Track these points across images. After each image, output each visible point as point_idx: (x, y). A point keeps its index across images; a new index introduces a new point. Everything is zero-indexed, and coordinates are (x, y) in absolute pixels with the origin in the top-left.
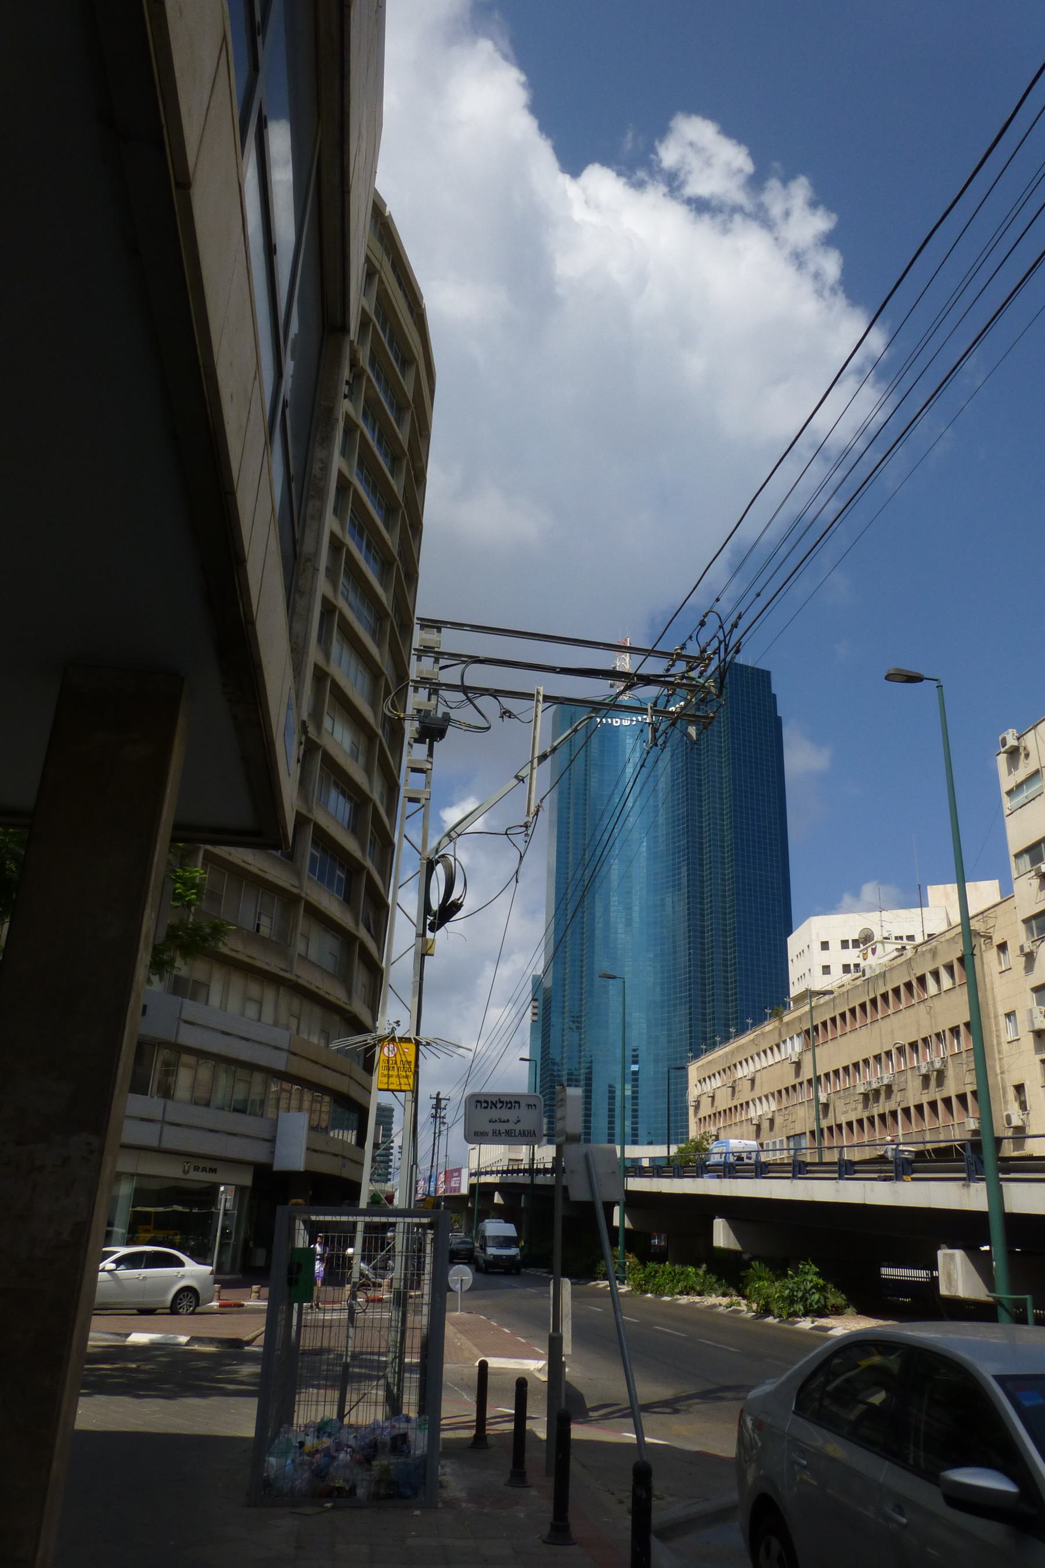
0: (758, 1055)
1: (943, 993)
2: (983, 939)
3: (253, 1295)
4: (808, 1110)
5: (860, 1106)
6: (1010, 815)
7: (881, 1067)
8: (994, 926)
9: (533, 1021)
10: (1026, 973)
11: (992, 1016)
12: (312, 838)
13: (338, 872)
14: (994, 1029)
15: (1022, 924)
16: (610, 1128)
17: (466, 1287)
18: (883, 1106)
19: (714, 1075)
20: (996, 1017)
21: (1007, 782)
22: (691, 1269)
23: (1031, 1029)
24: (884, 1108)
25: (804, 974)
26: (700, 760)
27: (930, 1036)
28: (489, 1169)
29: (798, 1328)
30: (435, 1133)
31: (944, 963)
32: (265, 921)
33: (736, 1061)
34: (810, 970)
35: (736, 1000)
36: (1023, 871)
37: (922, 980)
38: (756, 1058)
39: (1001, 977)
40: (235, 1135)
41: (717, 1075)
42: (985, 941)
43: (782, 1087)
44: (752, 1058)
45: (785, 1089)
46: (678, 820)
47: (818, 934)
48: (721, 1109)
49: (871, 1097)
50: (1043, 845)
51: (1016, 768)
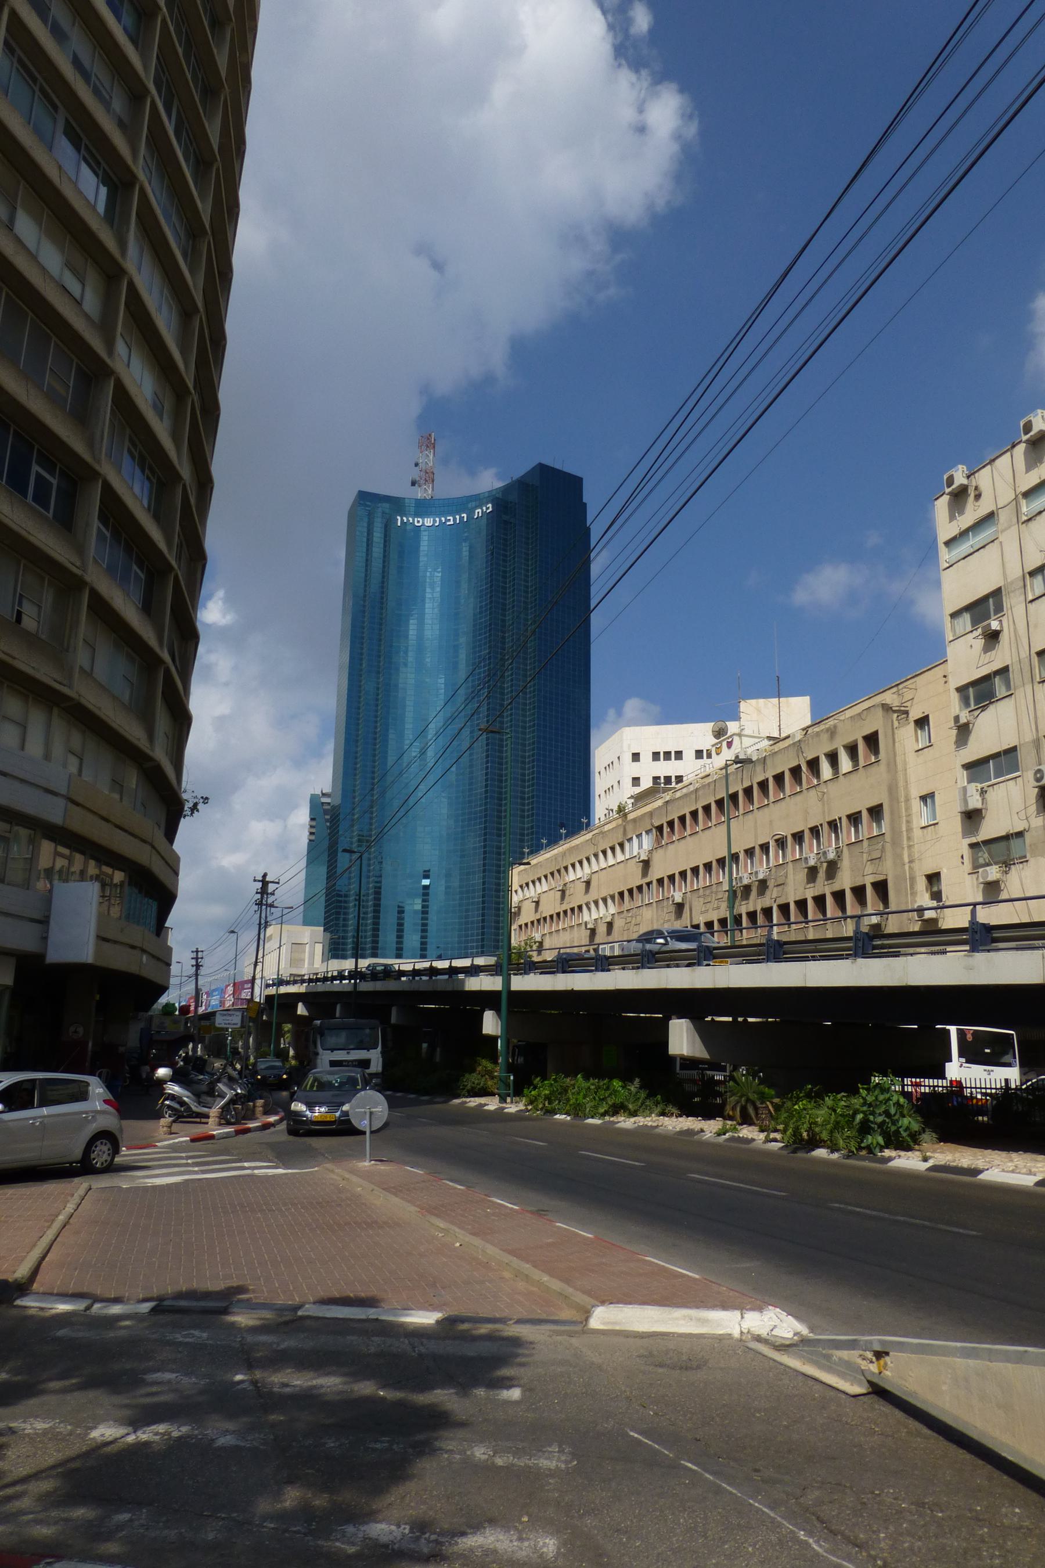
0: (596, 856)
1: (841, 776)
2: (895, 715)
4: (657, 910)
5: (724, 905)
7: (752, 863)
8: (913, 699)
9: (310, 840)
10: (957, 748)
11: (902, 799)
13: (135, 567)
14: (904, 813)
15: (956, 693)
16: (398, 943)
18: (755, 903)
19: (539, 879)
20: (907, 800)
21: (945, 527)
23: (963, 809)
25: (612, 786)
26: (505, 567)
27: (821, 825)
29: (980, 1179)
30: (260, 924)
31: (845, 742)
32: (28, 609)
33: (568, 862)
34: (619, 782)
36: (960, 631)
37: (814, 765)
38: (593, 859)
39: (918, 756)
41: (543, 879)
42: (898, 716)
43: (624, 888)
44: (588, 859)
47: (629, 746)
48: (547, 914)
49: (739, 894)
50: (991, 600)
51: (961, 512)
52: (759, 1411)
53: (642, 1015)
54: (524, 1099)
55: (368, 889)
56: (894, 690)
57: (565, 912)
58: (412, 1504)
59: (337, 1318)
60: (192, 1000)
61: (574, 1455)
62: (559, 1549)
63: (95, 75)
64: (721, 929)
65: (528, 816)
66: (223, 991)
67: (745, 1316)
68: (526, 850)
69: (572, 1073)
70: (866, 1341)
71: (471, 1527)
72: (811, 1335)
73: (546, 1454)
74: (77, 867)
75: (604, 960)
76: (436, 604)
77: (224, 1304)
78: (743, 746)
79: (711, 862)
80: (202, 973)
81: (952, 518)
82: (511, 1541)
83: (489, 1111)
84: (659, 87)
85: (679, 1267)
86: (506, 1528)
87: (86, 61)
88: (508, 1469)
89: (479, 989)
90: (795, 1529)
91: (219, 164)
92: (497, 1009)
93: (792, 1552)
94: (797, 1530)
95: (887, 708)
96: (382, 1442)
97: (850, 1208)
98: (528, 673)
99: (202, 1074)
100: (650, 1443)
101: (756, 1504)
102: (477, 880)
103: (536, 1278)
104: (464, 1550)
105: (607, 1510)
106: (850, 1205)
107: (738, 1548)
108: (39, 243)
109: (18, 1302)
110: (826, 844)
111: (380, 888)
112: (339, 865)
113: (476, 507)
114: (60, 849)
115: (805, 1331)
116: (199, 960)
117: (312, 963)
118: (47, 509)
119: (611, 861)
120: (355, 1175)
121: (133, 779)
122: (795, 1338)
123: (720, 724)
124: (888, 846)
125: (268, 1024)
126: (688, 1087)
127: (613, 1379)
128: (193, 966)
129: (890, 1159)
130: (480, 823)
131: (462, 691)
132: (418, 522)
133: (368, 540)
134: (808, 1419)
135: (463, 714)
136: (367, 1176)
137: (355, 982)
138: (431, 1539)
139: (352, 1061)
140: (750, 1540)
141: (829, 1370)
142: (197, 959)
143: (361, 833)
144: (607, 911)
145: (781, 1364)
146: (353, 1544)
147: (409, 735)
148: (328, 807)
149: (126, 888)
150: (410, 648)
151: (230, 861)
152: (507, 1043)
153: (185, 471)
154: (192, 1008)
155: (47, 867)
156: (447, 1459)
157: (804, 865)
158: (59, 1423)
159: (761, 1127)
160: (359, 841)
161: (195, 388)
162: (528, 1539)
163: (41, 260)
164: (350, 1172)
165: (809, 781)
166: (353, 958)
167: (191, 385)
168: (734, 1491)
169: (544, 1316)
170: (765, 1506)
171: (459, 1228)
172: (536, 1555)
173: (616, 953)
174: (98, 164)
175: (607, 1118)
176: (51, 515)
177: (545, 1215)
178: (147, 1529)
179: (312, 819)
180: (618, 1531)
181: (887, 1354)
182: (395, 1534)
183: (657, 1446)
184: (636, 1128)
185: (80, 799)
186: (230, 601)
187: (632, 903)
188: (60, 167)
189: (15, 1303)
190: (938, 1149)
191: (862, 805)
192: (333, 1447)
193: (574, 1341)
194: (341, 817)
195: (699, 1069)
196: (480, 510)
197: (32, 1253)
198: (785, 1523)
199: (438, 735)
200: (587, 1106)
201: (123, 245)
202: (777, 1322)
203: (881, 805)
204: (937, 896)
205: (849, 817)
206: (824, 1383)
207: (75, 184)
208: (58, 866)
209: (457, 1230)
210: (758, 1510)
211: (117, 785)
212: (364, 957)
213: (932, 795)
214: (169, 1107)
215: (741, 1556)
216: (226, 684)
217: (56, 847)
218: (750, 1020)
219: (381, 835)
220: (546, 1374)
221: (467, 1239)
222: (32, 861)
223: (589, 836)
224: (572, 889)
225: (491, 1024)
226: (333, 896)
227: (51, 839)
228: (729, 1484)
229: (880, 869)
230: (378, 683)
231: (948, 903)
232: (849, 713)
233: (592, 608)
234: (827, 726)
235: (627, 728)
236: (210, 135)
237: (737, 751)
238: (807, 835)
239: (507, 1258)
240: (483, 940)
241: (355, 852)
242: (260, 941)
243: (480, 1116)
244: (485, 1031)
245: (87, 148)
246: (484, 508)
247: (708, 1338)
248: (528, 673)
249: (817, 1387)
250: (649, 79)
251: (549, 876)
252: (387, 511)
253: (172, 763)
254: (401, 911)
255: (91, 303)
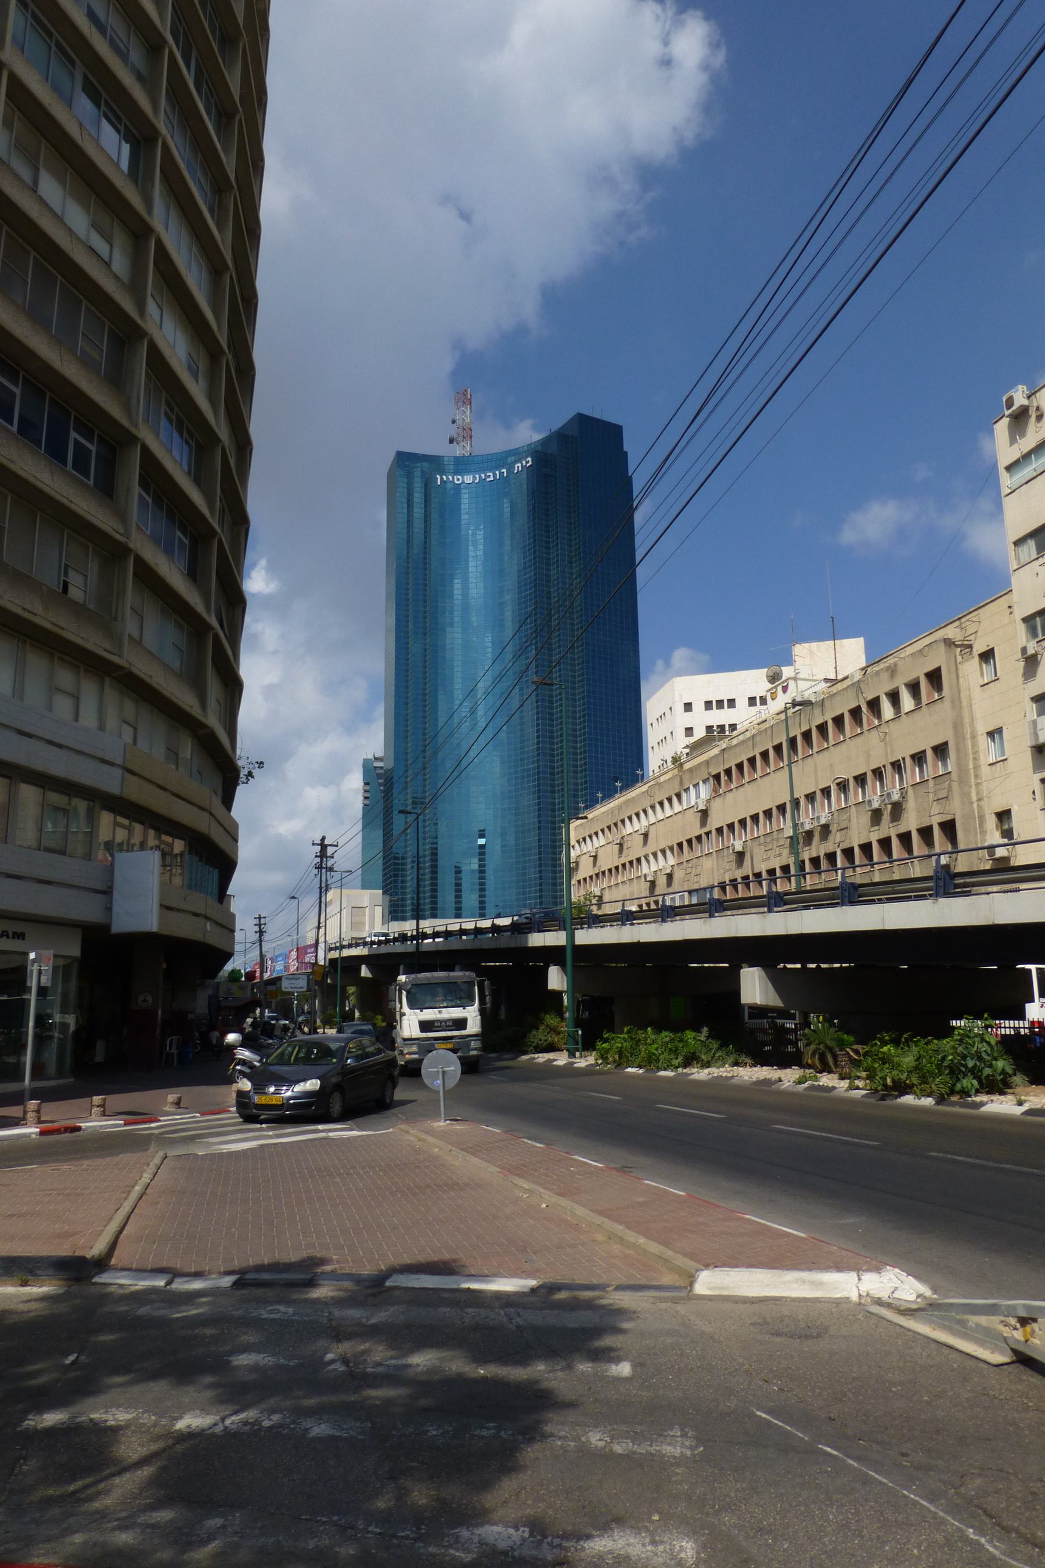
0: (653, 807)
1: (924, 707)
2: (959, 650)
3: (95, 1109)
5: (786, 852)
6: (1010, 493)
8: (976, 632)
9: (365, 805)
11: (969, 736)
12: (140, 473)
13: (179, 533)
17: (451, 1083)
18: (818, 849)
19: (596, 834)
20: (974, 737)
21: (1005, 450)
22: (690, 1035)
23: (1034, 744)
24: (818, 851)
27: (884, 766)
28: (333, 946)
30: (321, 888)
32: (75, 579)
34: (672, 733)
35: (585, 770)
36: (1024, 557)
37: (874, 705)
38: (650, 811)
39: (983, 691)
40: (49, 883)
41: (600, 833)
42: (961, 651)
43: (683, 839)
44: (645, 811)
45: (687, 841)
46: (526, 585)
47: (681, 696)
48: (605, 868)
51: (1023, 434)
52: (894, 1385)
53: (705, 965)
54: (594, 1053)
55: (424, 850)
56: (957, 623)
57: (624, 865)
58: (529, 1502)
59: (424, 1288)
60: (257, 967)
61: (700, 1440)
62: (698, 1553)
63: (111, 27)
64: (814, 871)
65: (581, 772)
66: (287, 957)
67: (863, 1277)
68: (582, 805)
69: (643, 1027)
70: (1009, 1306)
71: (596, 1528)
72: (935, 1296)
73: (669, 1439)
74: (136, 839)
75: (670, 910)
76: (479, 563)
77: (309, 1276)
78: (799, 690)
79: (771, 809)
80: (266, 939)
81: (1013, 441)
82: (644, 1545)
83: (558, 1067)
84: (683, 16)
85: (780, 1225)
86: (637, 1529)
87: (101, 14)
88: (628, 1456)
89: (542, 945)
90: (961, 1526)
91: (240, 115)
92: (562, 964)
93: (964, 1555)
94: (964, 1528)
95: (949, 643)
96: (488, 1429)
97: (949, 1156)
98: (576, 627)
99: (271, 1039)
100: (781, 1424)
101: (912, 1496)
102: (533, 838)
103: (632, 1240)
104: (593, 1557)
105: (745, 1505)
106: (949, 1153)
107: (901, 1550)
108: (64, 205)
109: (96, 1280)
110: (890, 785)
111: (436, 849)
112: (394, 827)
113: (516, 462)
114: (120, 819)
115: (928, 1293)
116: (262, 920)
117: (372, 925)
118: (88, 477)
119: (668, 812)
120: (430, 1135)
121: (187, 749)
122: (919, 1300)
123: (775, 669)
124: (955, 785)
125: (333, 987)
126: (761, 1037)
127: (728, 1351)
128: (256, 932)
129: (982, 1104)
130: (534, 781)
131: (509, 649)
132: (458, 479)
133: (408, 501)
134: (950, 1394)
135: (511, 671)
136: (443, 1136)
137: (418, 942)
138: (554, 1544)
139: (446, 1021)
140: (912, 1540)
141: (965, 1336)
142: (260, 925)
143: (415, 795)
144: (666, 863)
145: (909, 1330)
146: (468, 1551)
147: (459, 693)
148: (382, 771)
149: (187, 857)
150: (456, 608)
151: (286, 828)
152: (573, 999)
153: (223, 432)
154: (258, 974)
155: (107, 839)
156: (561, 1446)
157: (868, 808)
158: (143, 1413)
159: (841, 1074)
160: (414, 803)
161: (229, 348)
162: (662, 1542)
163: (68, 221)
164: (426, 1133)
165: (869, 722)
166: (413, 919)
167: (225, 345)
168: (884, 1480)
169: (644, 1282)
170: (922, 1498)
171: (545, 1188)
172: (673, 1562)
173: (677, 904)
174: (120, 120)
175: (680, 1070)
176: (91, 483)
177: (630, 1172)
178: (242, 1537)
179: (366, 784)
180: (761, 1529)
181: (1035, 1320)
182: (513, 1539)
183: (789, 1428)
184: (710, 1079)
185: (136, 769)
186: (272, 569)
187: (691, 853)
188: (81, 124)
189: (93, 1281)
190: (1031, 1092)
191: (926, 744)
192: (436, 1436)
193: (680, 1308)
194: (395, 779)
195: (768, 1018)
196: (520, 465)
197: (108, 1227)
198: (949, 1518)
199: (487, 694)
200: (661, 1057)
201: (149, 203)
202: (898, 1283)
203: (946, 743)
204: (1008, 834)
205: (913, 757)
206: (961, 1352)
207: (97, 141)
208: (118, 840)
209: (542, 1190)
210: (916, 1503)
211: (173, 754)
212: (424, 918)
213: (999, 730)
214: (240, 1071)
215: (906, 1560)
216: (275, 653)
217: (115, 818)
218: (823, 966)
219: (435, 796)
220: (654, 1346)
221: (553, 1200)
222: (91, 836)
223: (645, 788)
224: (629, 843)
225: (556, 979)
226: (391, 859)
227: (110, 809)
228: (876, 1472)
229: (947, 808)
230: (425, 644)
231: (1019, 840)
232: (909, 650)
233: (637, 562)
234: (887, 665)
235: (679, 679)
236: (231, 86)
237: (793, 695)
238: (870, 777)
239: (598, 1220)
240: (541, 897)
241: (410, 813)
242: (321, 905)
243: (549, 1072)
244: (550, 987)
245: (107, 103)
246: (524, 463)
247: (824, 1302)
248: (576, 627)
249: (954, 1355)
250: (674, 8)
251: (606, 830)
252: (426, 470)
253: (225, 730)
254: (458, 871)
255: (120, 264)
